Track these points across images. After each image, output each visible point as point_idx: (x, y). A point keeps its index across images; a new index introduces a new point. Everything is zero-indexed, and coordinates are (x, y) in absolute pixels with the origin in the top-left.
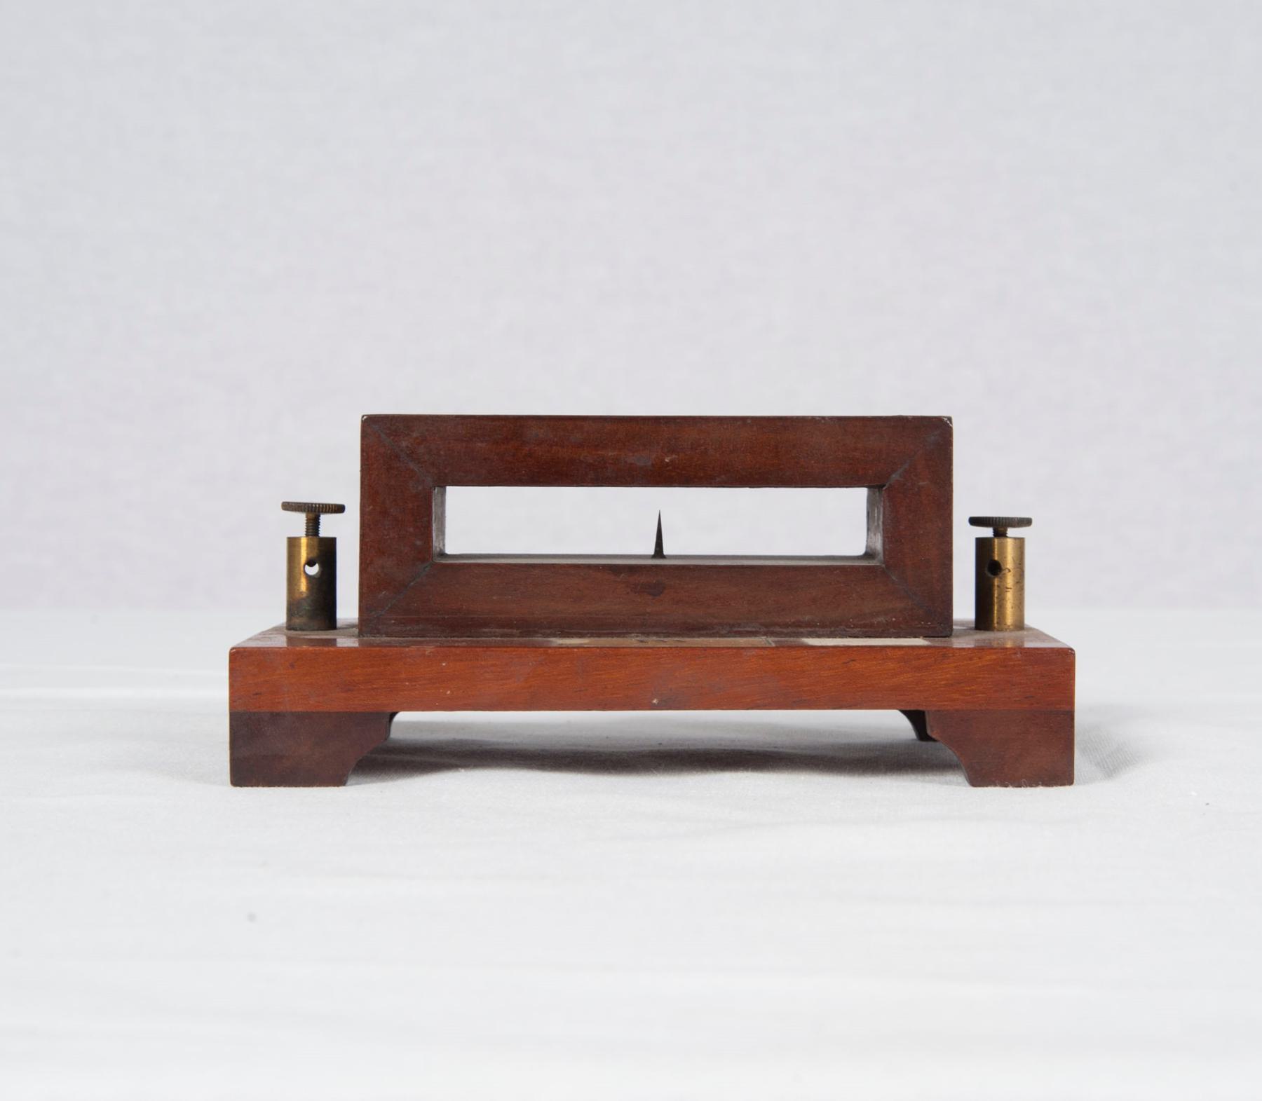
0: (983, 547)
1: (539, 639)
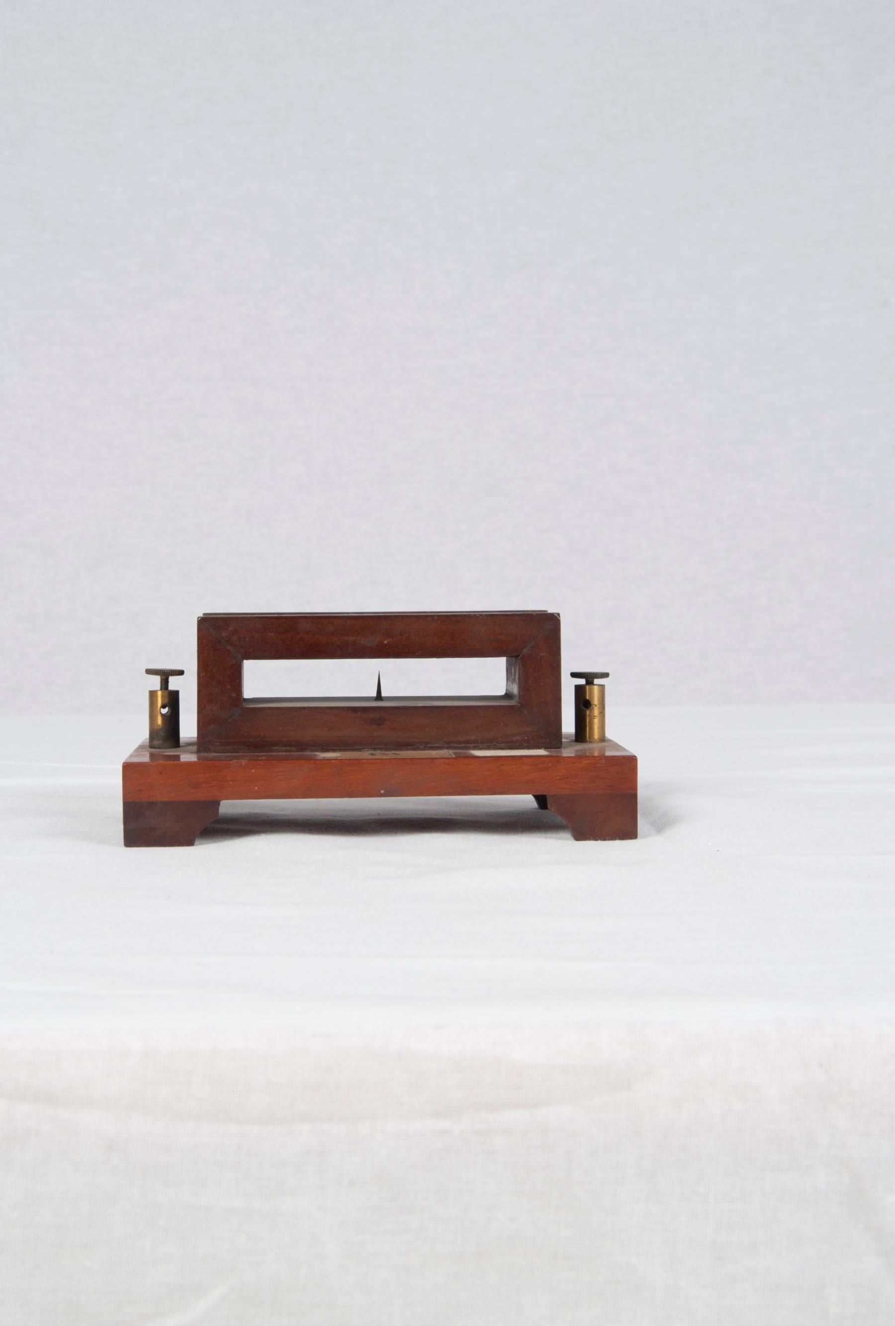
0: (579, 690)
1: (308, 753)
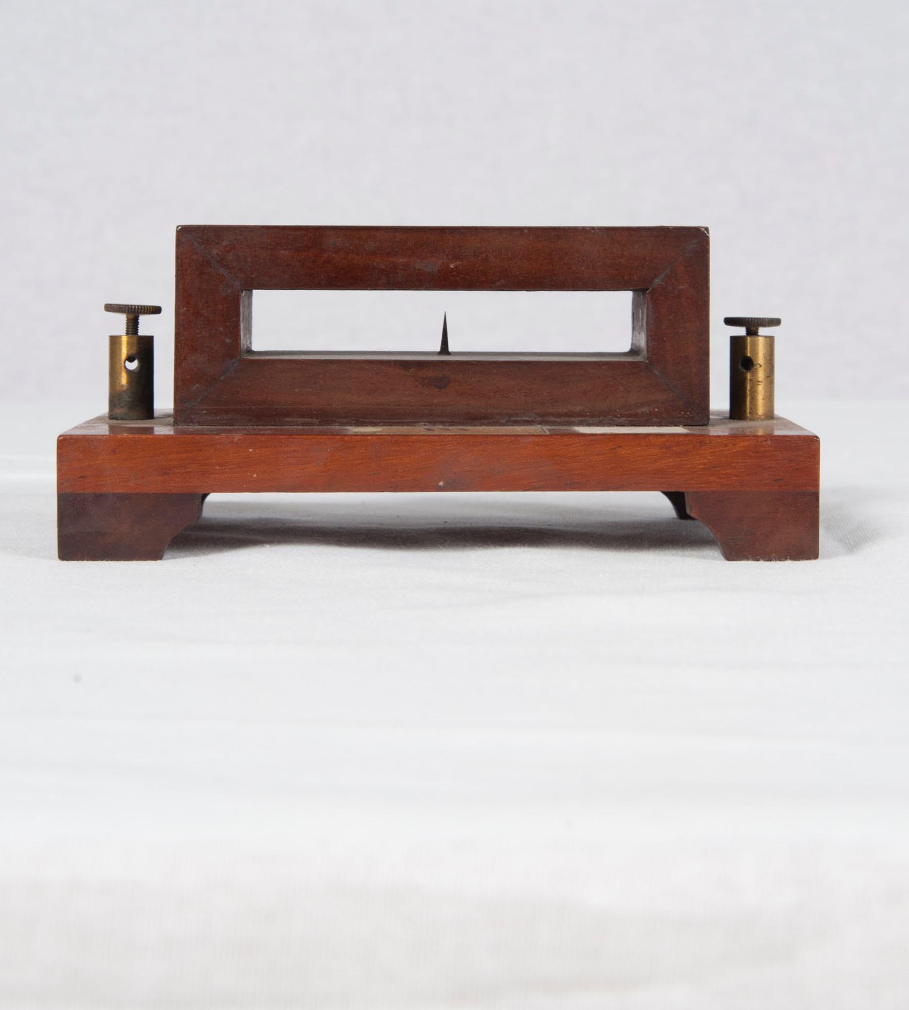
0: (736, 343)
1: (336, 428)
